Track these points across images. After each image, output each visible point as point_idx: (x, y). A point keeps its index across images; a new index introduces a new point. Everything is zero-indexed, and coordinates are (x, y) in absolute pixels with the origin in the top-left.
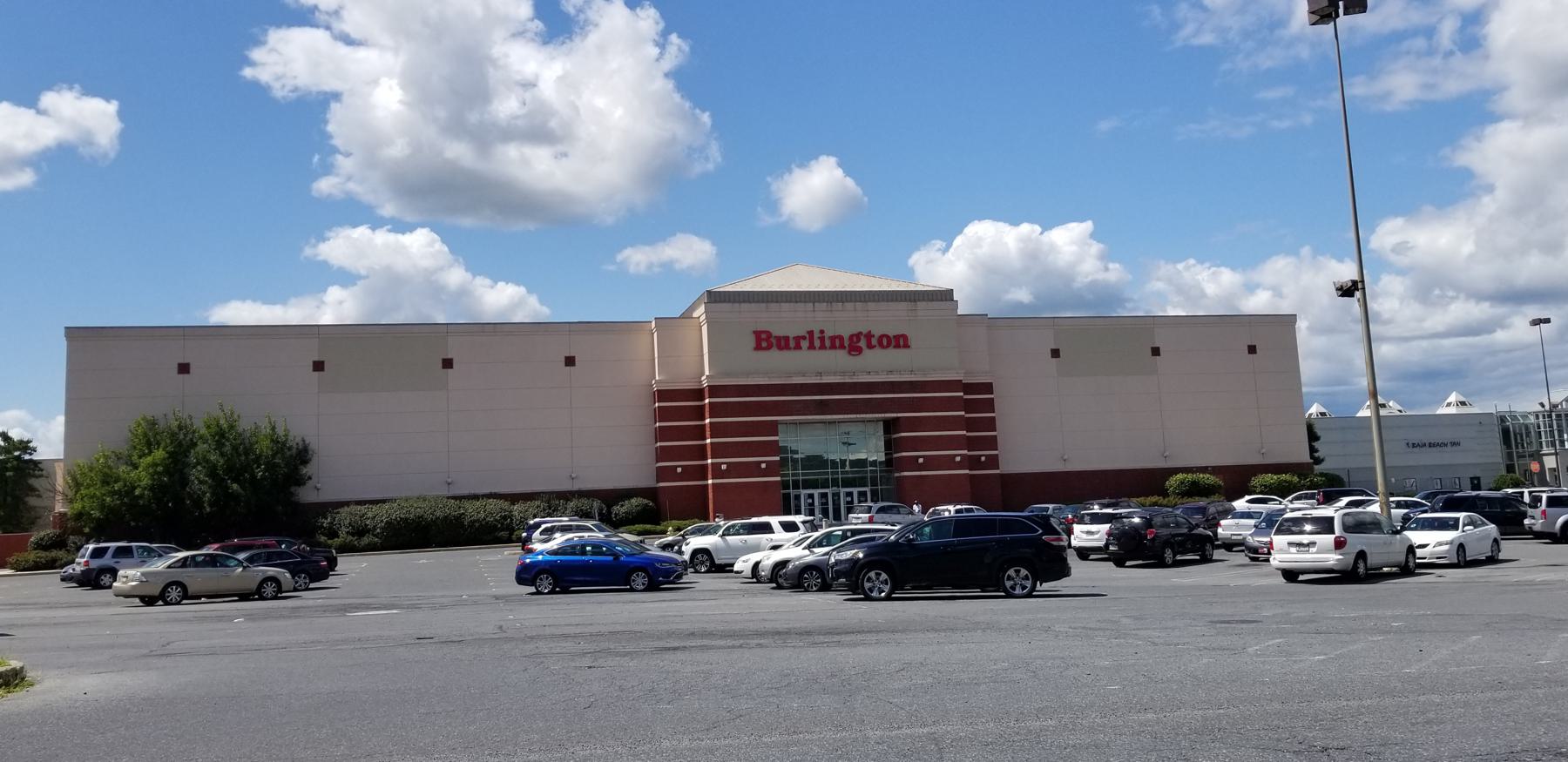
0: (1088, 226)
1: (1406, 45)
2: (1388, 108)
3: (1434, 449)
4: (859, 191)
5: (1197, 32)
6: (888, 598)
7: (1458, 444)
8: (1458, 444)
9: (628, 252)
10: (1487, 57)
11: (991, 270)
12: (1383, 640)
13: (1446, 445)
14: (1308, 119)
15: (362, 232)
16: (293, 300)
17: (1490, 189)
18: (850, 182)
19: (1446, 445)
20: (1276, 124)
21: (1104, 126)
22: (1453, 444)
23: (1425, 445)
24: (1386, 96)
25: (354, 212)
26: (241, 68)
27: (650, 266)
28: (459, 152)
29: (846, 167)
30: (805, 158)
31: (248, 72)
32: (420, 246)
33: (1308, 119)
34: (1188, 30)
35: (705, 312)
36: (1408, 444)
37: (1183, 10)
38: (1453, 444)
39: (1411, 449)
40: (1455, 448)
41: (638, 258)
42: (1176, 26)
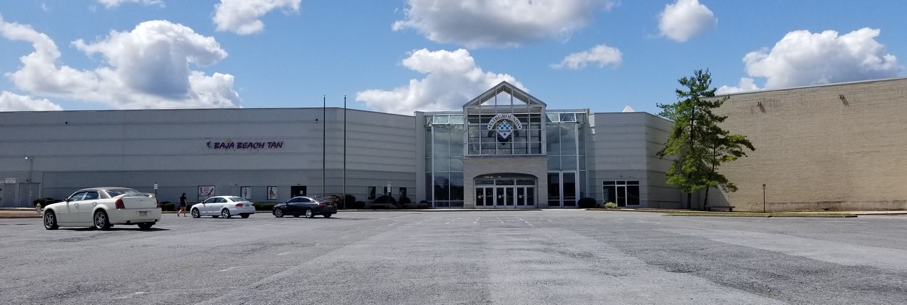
0: (876, 32)
3: (246, 151)
6: (312, 217)
7: (279, 145)
8: (279, 145)
9: (567, 59)
11: (801, 67)
12: (219, 270)
13: (261, 145)
15: (424, 52)
16: (397, 89)
18: (703, 7)
19: (261, 145)
22: (217, 146)
23: (232, 145)
25: (417, 41)
26: (881, 33)
27: (580, 64)
31: (876, 32)
32: (460, 58)
36: (208, 144)
38: (217, 146)
39: (213, 151)
40: (273, 150)
41: (574, 60)
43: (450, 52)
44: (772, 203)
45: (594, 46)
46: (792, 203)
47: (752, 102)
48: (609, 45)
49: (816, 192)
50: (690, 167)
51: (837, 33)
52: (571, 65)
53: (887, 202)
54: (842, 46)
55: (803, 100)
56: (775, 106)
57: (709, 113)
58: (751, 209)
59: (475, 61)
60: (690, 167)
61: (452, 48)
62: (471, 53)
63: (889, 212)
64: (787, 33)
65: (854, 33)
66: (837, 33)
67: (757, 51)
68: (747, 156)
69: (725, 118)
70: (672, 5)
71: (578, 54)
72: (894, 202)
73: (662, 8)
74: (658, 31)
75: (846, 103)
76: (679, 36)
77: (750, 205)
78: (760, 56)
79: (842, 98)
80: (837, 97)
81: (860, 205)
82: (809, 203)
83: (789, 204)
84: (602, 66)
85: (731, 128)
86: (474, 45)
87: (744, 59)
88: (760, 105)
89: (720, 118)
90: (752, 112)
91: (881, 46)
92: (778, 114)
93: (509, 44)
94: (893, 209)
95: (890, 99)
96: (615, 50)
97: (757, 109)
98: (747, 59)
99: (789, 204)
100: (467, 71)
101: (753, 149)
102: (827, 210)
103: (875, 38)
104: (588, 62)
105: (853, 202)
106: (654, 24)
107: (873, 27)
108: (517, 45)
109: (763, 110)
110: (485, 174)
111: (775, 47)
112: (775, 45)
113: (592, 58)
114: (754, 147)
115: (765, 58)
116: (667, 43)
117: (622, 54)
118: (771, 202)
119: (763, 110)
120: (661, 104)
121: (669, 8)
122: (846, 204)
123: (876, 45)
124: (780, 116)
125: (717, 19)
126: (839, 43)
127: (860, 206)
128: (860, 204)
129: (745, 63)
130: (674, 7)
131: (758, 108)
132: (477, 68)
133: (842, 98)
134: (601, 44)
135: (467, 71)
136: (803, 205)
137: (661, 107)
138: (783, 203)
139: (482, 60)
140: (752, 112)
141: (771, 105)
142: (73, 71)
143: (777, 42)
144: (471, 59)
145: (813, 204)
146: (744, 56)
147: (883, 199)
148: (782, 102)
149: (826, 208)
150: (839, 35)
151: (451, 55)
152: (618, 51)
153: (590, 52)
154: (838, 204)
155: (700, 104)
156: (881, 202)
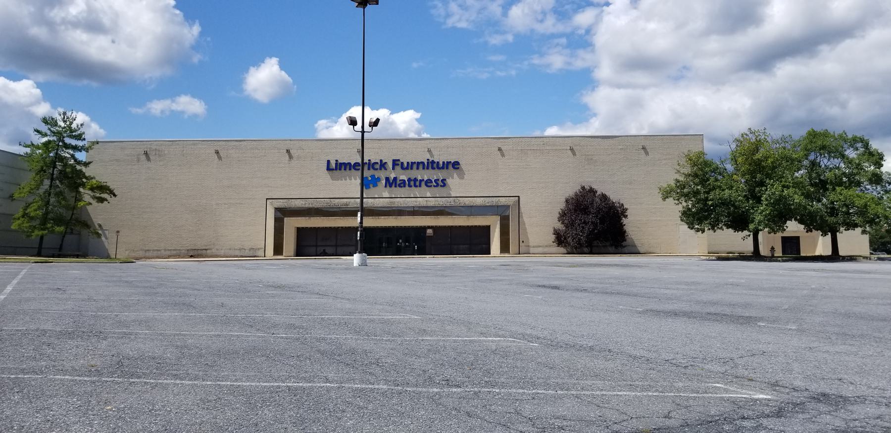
0: (418, 115)
1: (556, 41)
2: (548, 71)
4: (289, 79)
5: (460, 20)
7: (503, 155)
10: (593, 51)
14: (513, 73)
17: (595, 115)
18: (283, 73)
20: (499, 73)
21: (415, 65)
24: (548, 66)
26: (201, 25)
27: (162, 112)
28: (38, 32)
29: (282, 66)
30: (258, 62)
31: (418, 115)
33: (513, 73)
34: (455, 18)
35: (38, 248)
37: (453, 7)
41: (157, 107)
42: (448, 15)
43: (12, 81)
44: (148, 250)
45: (179, 94)
46: (165, 250)
47: (139, 150)
48: (193, 96)
49: (187, 239)
50: (36, 210)
51: (390, 112)
52: (153, 111)
53: (245, 250)
54: (392, 123)
55: (184, 152)
56: (160, 156)
57: (73, 156)
58: (128, 255)
59: (42, 94)
60: (36, 210)
61: (16, 78)
62: (39, 85)
63: (224, 259)
64: (353, 106)
65: (402, 113)
66: (390, 112)
67: (327, 119)
68: (109, 203)
69: (90, 163)
70: (256, 68)
71: (162, 101)
72: (251, 249)
73: (247, 70)
74: (242, 90)
75: (220, 158)
76: (261, 96)
77: (127, 252)
78: (329, 124)
79: (217, 152)
80: (213, 152)
81: (222, 252)
82: (180, 250)
83: (163, 251)
84: (186, 116)
85: (97, 172)
86: (42, 77)
87: (316, 125)
88: (146, 154)
89: (85, 162)
90: (138, 161)
91: (420, 126)
92: (161, 163)
93: (85, 82)
94: (248, 255)
95: (255, 157)
96: (200, 102)
97: (143, 157)
98: (319, 125)
99: (163, 251)
100: (32, 104)
101: (115, 195)
102: (191, 256)
103: (417, 120)
104: (172, 111)
105: (217, 249)
106: (239, 83)
107: (417, 111)
108: (94, 84)
109: (148, 159)
110: (858, 255)
111: (342, 117)
112: (342, 116)
113: (175, 107)
114: (116, 194)
115: (332, 127)
116: (250, 103)
117: (206, 107)
118: (147, 248)
119: (148, 159)
120: (25, 143)
121: (252, 70)
122: (211, 251)
123: (417, 125)
124: (163, 166)
125: (295, 87)
126: (390, 120)
127: (222, 253)
128: (223, 251)
129: (317, 129)
130: (257, 69)
131: (144, 156)
132: (45, 102)
133: (217, 152)
134: (186, 94)
135: (32, 104)
136: (175, 252)
137: (24, 147)
138: (157, 250)
139: (48, 92)
140: (138, 161)
141: (156, 154)
142: (6, 80)
143: (344, 113)
144: (38, 92)
145: (183, 251)
146: (316, 122)
147: (242, 247)
148: (166, 152)
149: (190, 255)
150: (390, 114)
151: (12, 85)
152: (203, 103)
153: (173, 101)
154: (205, 251)
155: (67, 146)
156: (240, 250)
